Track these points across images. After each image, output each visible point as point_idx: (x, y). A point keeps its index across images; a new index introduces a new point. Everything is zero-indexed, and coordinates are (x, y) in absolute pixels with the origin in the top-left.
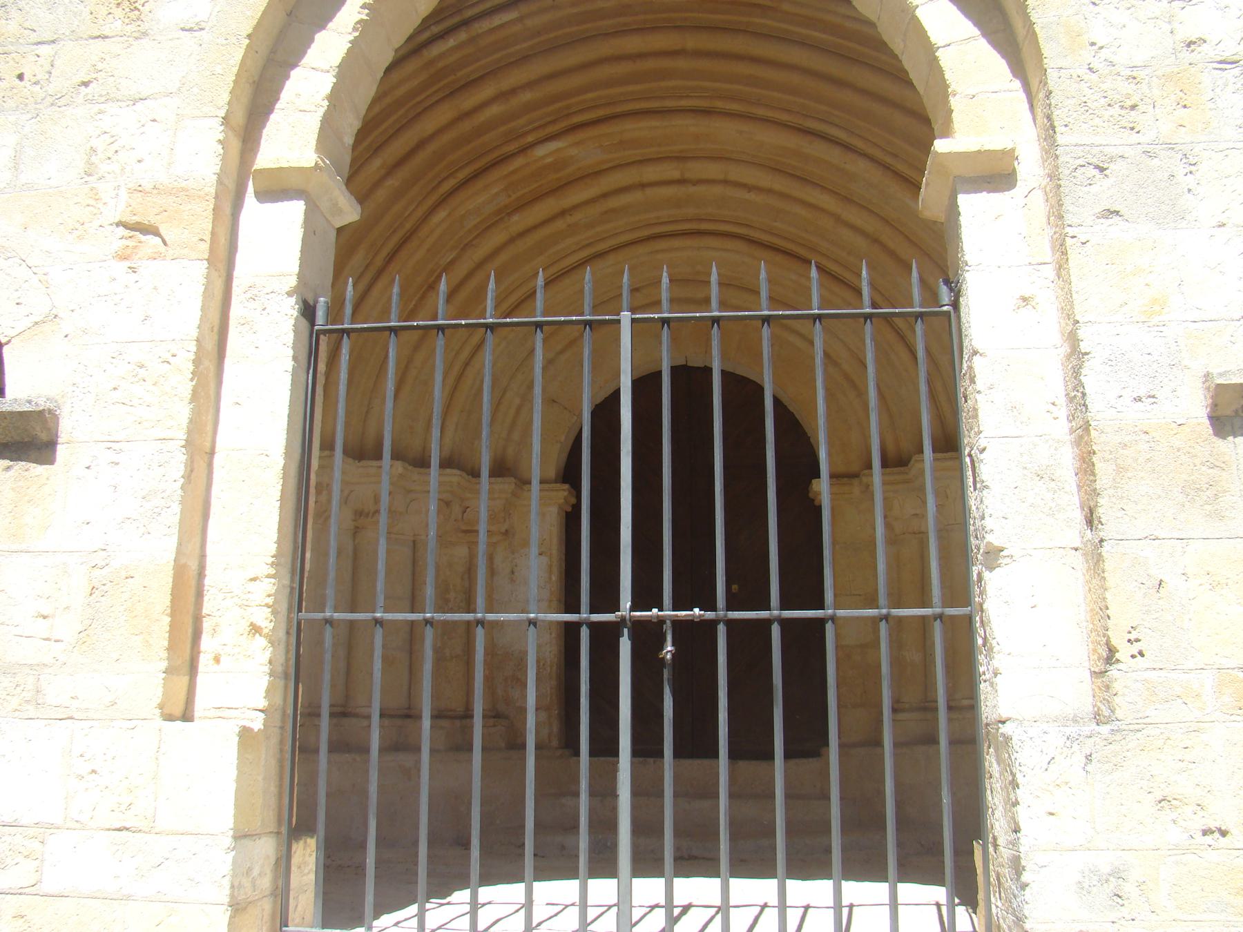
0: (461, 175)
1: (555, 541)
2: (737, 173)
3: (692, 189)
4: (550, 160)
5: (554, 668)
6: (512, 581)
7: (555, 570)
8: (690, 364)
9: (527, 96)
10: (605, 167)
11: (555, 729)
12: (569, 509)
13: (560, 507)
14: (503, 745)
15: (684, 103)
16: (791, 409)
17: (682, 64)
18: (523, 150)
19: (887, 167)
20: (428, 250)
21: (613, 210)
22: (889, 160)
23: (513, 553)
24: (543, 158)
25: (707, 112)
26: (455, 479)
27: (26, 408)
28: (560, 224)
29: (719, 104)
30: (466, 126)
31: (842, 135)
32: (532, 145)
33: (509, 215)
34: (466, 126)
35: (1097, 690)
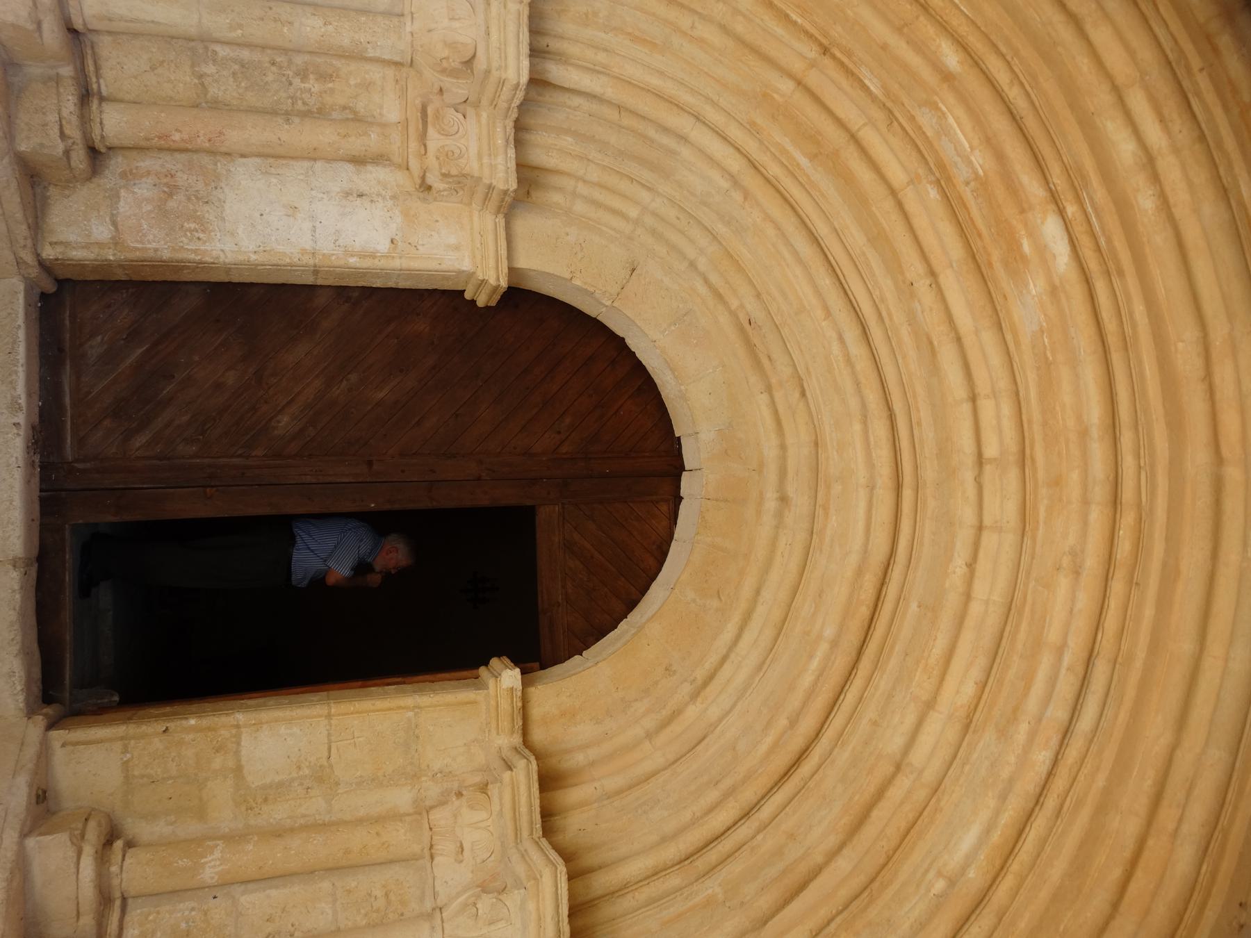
0: (1013, 93)
1: (415, 265)
3: (968, 476)
4: (1026, 247)
6: (347, 194)
8: (685, 478)
9: (1146, 202)
10: (1009, 337)
11: (77, 254)
12: (468, 296)
13: (471, 275)
16: (623, 625)
18: (1054, 198)
20: (884, 47)
23: (394, 197)
24: (1033, 234)
27: (309, 280)
28: (914, 269)
29: (1127, 520)
31: (1086, 722)
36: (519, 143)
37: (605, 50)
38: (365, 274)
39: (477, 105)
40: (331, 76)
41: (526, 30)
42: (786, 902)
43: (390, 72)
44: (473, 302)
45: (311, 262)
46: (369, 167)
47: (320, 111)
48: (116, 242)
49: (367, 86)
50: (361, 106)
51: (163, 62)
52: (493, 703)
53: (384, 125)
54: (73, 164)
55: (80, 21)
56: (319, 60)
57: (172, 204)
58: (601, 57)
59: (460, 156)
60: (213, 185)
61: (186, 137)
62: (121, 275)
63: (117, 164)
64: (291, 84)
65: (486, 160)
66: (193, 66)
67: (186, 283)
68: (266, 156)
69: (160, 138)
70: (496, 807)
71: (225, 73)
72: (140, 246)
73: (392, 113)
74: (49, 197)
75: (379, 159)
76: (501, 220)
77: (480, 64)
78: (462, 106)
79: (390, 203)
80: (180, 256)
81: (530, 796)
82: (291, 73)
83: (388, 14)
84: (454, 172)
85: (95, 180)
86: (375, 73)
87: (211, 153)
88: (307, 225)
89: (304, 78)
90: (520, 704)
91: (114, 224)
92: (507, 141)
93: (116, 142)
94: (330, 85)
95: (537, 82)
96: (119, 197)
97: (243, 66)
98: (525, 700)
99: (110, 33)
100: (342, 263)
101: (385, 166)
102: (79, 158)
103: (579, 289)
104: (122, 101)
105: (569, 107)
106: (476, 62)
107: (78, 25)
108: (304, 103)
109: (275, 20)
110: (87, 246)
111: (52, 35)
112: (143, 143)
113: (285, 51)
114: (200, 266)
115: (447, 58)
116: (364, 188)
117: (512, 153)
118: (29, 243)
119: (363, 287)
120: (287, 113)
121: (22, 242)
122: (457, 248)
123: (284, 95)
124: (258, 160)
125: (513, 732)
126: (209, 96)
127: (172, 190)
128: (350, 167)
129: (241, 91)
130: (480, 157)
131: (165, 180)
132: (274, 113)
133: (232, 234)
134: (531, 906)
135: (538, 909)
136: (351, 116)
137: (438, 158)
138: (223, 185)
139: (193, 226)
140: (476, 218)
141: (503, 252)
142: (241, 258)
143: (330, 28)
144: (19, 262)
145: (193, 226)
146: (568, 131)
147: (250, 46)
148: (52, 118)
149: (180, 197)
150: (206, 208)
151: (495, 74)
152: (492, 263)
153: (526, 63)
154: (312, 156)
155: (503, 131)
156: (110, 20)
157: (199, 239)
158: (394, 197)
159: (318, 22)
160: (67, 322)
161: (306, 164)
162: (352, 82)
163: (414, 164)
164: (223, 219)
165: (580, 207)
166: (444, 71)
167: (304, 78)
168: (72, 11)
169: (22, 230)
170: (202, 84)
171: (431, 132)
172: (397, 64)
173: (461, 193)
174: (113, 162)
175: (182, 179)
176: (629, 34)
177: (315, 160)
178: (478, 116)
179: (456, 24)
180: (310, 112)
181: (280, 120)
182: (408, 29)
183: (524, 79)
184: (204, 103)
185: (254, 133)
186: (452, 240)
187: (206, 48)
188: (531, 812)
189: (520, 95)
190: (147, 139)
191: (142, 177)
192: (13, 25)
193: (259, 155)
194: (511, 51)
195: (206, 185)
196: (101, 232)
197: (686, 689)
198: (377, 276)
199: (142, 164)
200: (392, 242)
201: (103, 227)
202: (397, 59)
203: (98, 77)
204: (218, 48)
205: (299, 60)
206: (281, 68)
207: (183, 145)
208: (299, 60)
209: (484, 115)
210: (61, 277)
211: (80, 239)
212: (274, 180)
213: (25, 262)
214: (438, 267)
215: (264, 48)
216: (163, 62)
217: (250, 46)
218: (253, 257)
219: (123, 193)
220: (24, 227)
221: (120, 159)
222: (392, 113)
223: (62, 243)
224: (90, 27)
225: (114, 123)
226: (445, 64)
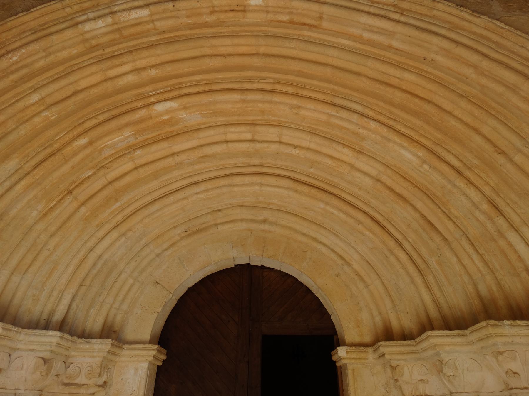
0: (101, 118)
2: (288, 136)
3: (258, 146)
8: (252, 263)
9: (153, 73)
10: (202, 126)
12: (160, 364)
15: (256, 86)
16: (318, 295)
17: (255, 61)
19: (390, 127)
20: (73, 167)
21: (206, 156)
22: (391, 123)
24: (161, 114)
25: (271, 92)
26: (55, 340)
28: (170, 161)
29: (278, 87)
30: (109, 86)
31: (359, 108)
32: (153, 103)
33: (134, 150)
34: (109, 86)
37: (52, 292)
39: (68, 357)
42: (436, 229)
44: (164, 361)
52: (353, 361)
58: (55, 293)
65: (95, 354)
70: (402, 362)
76: (126, 346)
78: (67, 364)
81: (396, 346)
84: (98, 370)
90: (354, 348)
92: (87, 342)
98: (352, 345)
103: (163, 309)
105: (77, 310)
115: (41, 372)
122: (136, 369)
125: (366, 352)
130: (93, 357)
134: (447, 348)
135: (449, 345)
137: (91, 378)
140: (123, 359)
146: (88, 311)
151: (53, 348)
152: (146, 352)
153: (51, 332)
155: (82, 344)
165: (125, 307)
166: (47, 374)
171: (77, 381)
178: (73, 356)
179: (25, 367)
182: (22, 392)
188: (404, 346)
189: (66, 336)
194: (43, 339)
197: (346, 268)
209: (73, 353)
214: (145, 380)
226: (44, 374)
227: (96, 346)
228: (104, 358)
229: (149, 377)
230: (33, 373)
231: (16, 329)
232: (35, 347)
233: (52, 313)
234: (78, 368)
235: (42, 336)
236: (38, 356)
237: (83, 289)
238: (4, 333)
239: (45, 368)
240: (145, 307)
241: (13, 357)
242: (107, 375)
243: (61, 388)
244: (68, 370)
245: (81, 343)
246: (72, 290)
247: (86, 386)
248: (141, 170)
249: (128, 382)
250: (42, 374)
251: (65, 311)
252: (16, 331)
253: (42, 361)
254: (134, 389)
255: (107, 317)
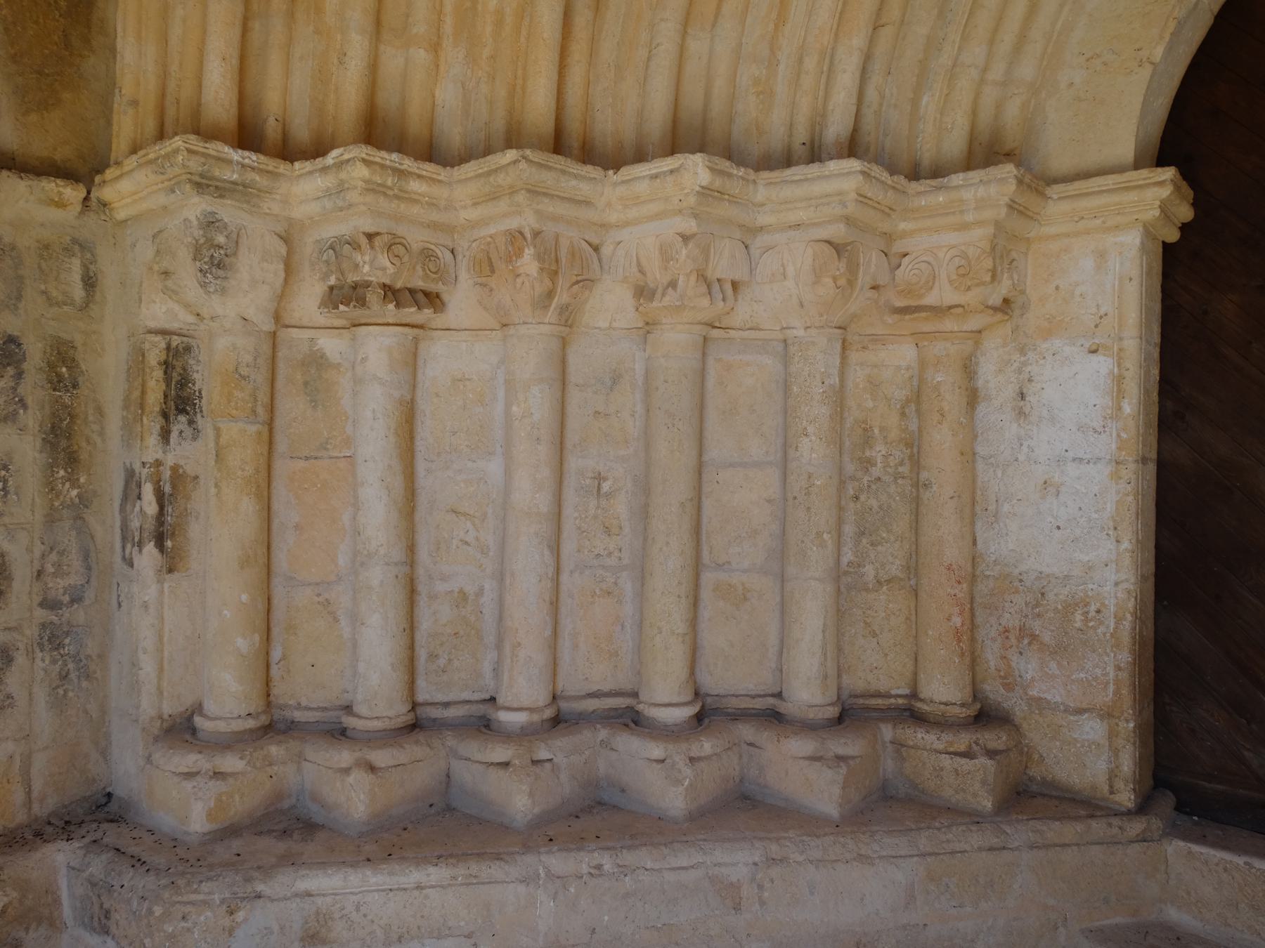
5: (1127, 624)
6: (1021, 414)
7: (1133, 389)
12: (1173, 236)
13: (1148, 233)
14: (987, 804)
23: (1022, 351)
26: (850, 185)
27: (1152, 467)
35: (98, 440)
36: (938, 172)
37: (800, 61)
38: (1147, 392)
39: (889, 237)
40: (865, 430)
41: (788, 172)
43: (854, 356)
44: (1184, 228)
45: (1132, 466)
46: (980, 383)
47: (909, 445)
48: (1107, 714)
49: (874, 385)
50: (900, 394)
51: (866, 623)
53: (923, 364)
54: (1002, 747)
55: (831, 709)
56: (847, 444)
57: (1047, 637)
58: (810, 63)
59: (964, 255)
60: (1016, 583)
61: (957, 610)
62: (1149, 712)
63: (994, 690)
64: (879, 479)
65: (970, 217)
66: (867, 590)
67: (1156, 632)
68: (974, 515)
69: (959, 641)
71: (873, 556)
72: (1111, 688)
73: (902, 355)
74: (1043, 778)
75: (969, 369)
76: (1055, 191)
77: (837, 231)
78: (894, 260)
79: (1031, 355)
80: (1126, 638)
82: (866, 479)
83: (786, 359)
84: (988, 263)
85: (1017, 721)
86: (857, 376)
87: (973, 578)
88: (1072, 470)
89: (870, 462)
91: (1080, 711)
92: (939, 188)
93: (969, 690)
94: (876, 431)
95: (852, 147)
96: (1040, 698)
97: (863, 533)
99: (839, 676)
100: (1131, 423)
101: (977, 364)
102: (995, 738)
103: (1169, 49)
104: (915, 674)
105: (881, 105)
106: (835, 240)
107: (833, 712)
108: (901, 464)
109: (808, 494)
110: (1116, 752)
111: (849, 745)
112: (967, 660)
113: (842, 484)
114: (1138, 617)
115: (835, 279)
116: (1010, 391)
117: (957, 179)
118: (1116, 821)
119: (1160, 393)
120: (916, 485)
121: (1115, 830)
122: (1101, 255)
123: (893, 487)
124: (979, 525)
126: (902, 576)
127: (1027, 635)
128: (981, 409)
129: (892, 538)
130: (964, 227)
131: (1013, 641)
132: (917, 501)
133: (1090, 568)
136: (913, 406)
137: (969, 289)
138: (1017, 571)
139: (1078, 617)
140: (1052, 230)
141: (1110, 181)
142: (1127, 561)
143: (810, 429)
144: (1143, 839)
145: (1078, 617)
146: (915, 102)
147: (840, 522)
148: (946, 761)
149: (1036, 626)
150: (1051, 596)
151: (851, 208)
152: (1132, 196)
153: (833, 166)
154: (969, 457)
155: (926, 196)
156: (826, 677)
157: (1098, 612)
158: (1022, 351)
159: (805, 444)
160: (1220, 787)
161: (980, 466)
162: (870, 404)
163: (974, 323)
164: (1067, 577)
165: (1027, 70)
166: (851, 283)
167: (870, 462)
168: (820, 716)
169: (1098, 827)
170: (888, 581)
171: (930, 299)
172: (845, 346)
173: (1014, 255)
174: (991, 696)
175: (1010, 619)
176: (776, 26)
177: (974, 454)
178: (904, 235)
179: (790, 270)
180: (911, 457)
181: (926, 495)
182: (801, 333)
183: (854, 164)
184: (912, 578)
185: (944, 527)
186: (1088, 263)
187: (846, 573)
189: (877, 171)
190: (963, 654)
191: (1010, 666)
192: (843, 788)
193: (973, 524)
194: (818, 188)
195: (1017, 592)
196: (1092, 729)
198: (1147, 373)
199: (992, 664)
200: (1094, 352)
201: (1089, 725)
202: (838, 346)
203: (887, 696)
204: (845, 560)
205: (850, 468)
206: (861, 490)
207: (967, 614)
208: (850, 468)
209: (903, 226)
210: (1152, 782)
211: (1105, 757)
212: (1006, 508)
213: (1144, 831)
214: (1135, 283)
215: (841, 509)
216: (866, 623)
217: (840, 522)
218: (1126, 545)
219: (1034, 692)
220: (1094, 824)
221: (987, 687)
222: (902, 355)
223: (1110, 779)
224: (835, 698)
225: (943, 689)
226: (842, 282)
227: (968, 195)
228: (998, 225)
229: (1148, 274)
230: (814, 283)
231: (741, 172)
232: (801, 215)
233: (819, 120)
234: (923, 266)
235: (813, 179)
236: (819, 238)
237: (886, 34)
238: (718, 183)
239: (842, 266)
240: (1098, 56)
241: (755, 252)
242: (1012, 279)
243: (890, 321)
244: (899, 273)
245: (919, 193)
246: (857, 41)
247: (960, 310)
248: (685, 864)
249: (1077, 292)
250: (839, 283)
251: (854, 109)
252: (743, 179)
253: (828, 250)
254: (1102, 312)
255: (974, 113)
